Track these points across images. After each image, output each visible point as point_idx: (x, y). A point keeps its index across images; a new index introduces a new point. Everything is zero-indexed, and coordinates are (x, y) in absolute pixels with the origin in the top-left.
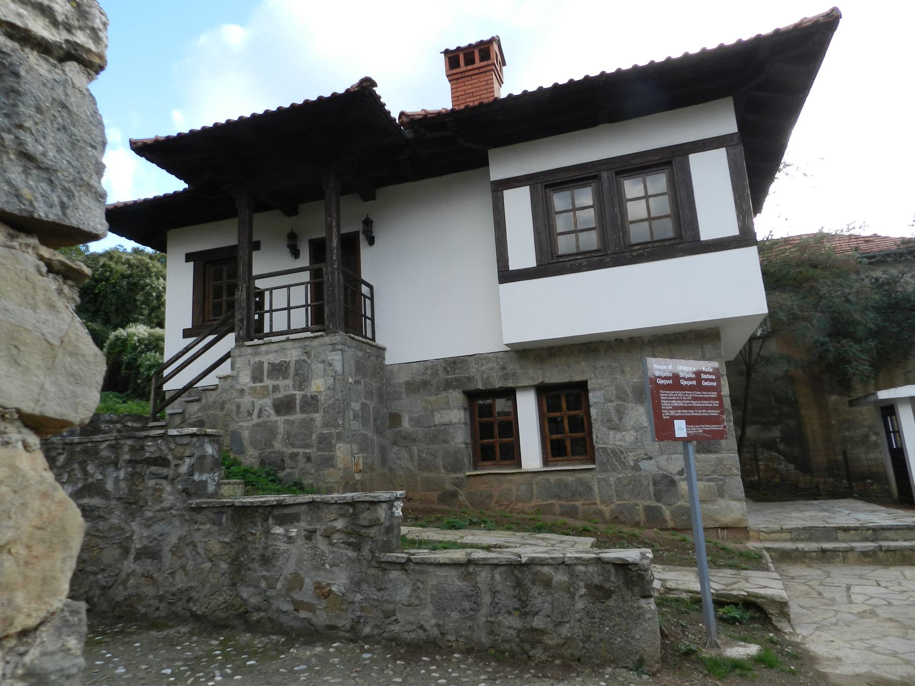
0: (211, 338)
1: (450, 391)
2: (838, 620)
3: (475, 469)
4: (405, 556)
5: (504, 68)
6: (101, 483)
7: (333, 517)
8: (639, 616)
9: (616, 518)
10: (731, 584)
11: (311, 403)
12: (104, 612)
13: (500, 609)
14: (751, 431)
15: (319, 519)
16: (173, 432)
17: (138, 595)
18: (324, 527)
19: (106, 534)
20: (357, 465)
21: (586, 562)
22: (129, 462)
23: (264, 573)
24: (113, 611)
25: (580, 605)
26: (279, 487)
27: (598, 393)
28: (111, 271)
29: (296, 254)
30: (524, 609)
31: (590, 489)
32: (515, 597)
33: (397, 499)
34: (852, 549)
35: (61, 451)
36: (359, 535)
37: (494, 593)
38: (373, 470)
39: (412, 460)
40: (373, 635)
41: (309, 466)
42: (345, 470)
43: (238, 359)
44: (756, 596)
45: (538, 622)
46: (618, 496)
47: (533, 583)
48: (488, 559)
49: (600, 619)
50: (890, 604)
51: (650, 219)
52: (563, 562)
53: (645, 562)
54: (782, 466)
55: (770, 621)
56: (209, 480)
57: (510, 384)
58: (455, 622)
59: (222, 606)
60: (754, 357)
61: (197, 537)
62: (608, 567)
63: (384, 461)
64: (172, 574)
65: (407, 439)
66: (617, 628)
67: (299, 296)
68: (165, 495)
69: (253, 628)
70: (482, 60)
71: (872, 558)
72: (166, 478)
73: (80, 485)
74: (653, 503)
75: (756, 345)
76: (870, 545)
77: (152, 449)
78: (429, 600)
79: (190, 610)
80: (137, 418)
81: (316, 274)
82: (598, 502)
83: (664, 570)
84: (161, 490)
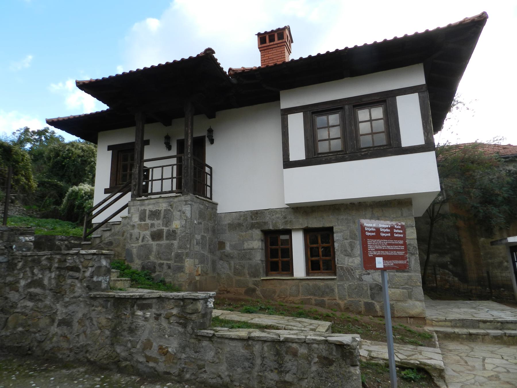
0: (119, 194)
1: (254, 230)
2: (476, 381)
3: (267, 275)
4: (212, 332)
5: (292, 44)
6: (41, 280)
7: (172, 306)
8: (348, 377)
9: (348, 308)
10: (410, 356)
11: (172, 235)
12: (38, 356)
13: (266, 368)
14: (433, 257)
15: (163, 308)
16: (83, 252)
17: (58, 347)
18: (166, 312)
19: (42, 310)
20: (197, 271)
21: (319, 342)
22: (58, 268)
23: (130, 338)
24: (44, 356)
25: (314, 368)
26: (151, 283)
27: (340, 234)
28: (72, 153)
29: (169, 148)
30: (281, 369)
31: (333, 290)
32: (275, 361)
33: (210, 297)
34: (488, 334)
35: (20, 260)
36: (186, 319)
37: (263, 358)
38: (207, 274)
39: (230, 269)
40: (191, 380)
41: (169, 271)
42: (190, 274)
43: (132, 208)
44: (425, 364)
45: (288, 377)
46: (349, 296)
47: (286, 353)
48: (260, 337)
49: (326, 378)
50: (508, 372)
51: (372, 133)
52: (305, 342)
53: (355, 344)
54: (450, 279)
55: (433, 380)
56: (103, 281)
57: (288, 227)
58: (240, 374)
59: (105, 357)
60: (435, 214)
61: (93, 315)
62: (332, 346)
63: (214, 269)
64: (78, 336)
65: (227, 257)
66: (336, 384)
67: (168, 173)
68: (76, 289)
69: (122, 371)
70: (279, 39)
71: (499, 340)
72: (77, 278)
73: (29, 281)
74: (370, 301)
75: (437, 207)
76: (499, 332)
77: (71, 261)
78: (225, 360)
79: (87, 358)
80: (78, 238)
81: (180, 160)
82: (337, 298)
83: (371, 344)
84: (74, 286)
